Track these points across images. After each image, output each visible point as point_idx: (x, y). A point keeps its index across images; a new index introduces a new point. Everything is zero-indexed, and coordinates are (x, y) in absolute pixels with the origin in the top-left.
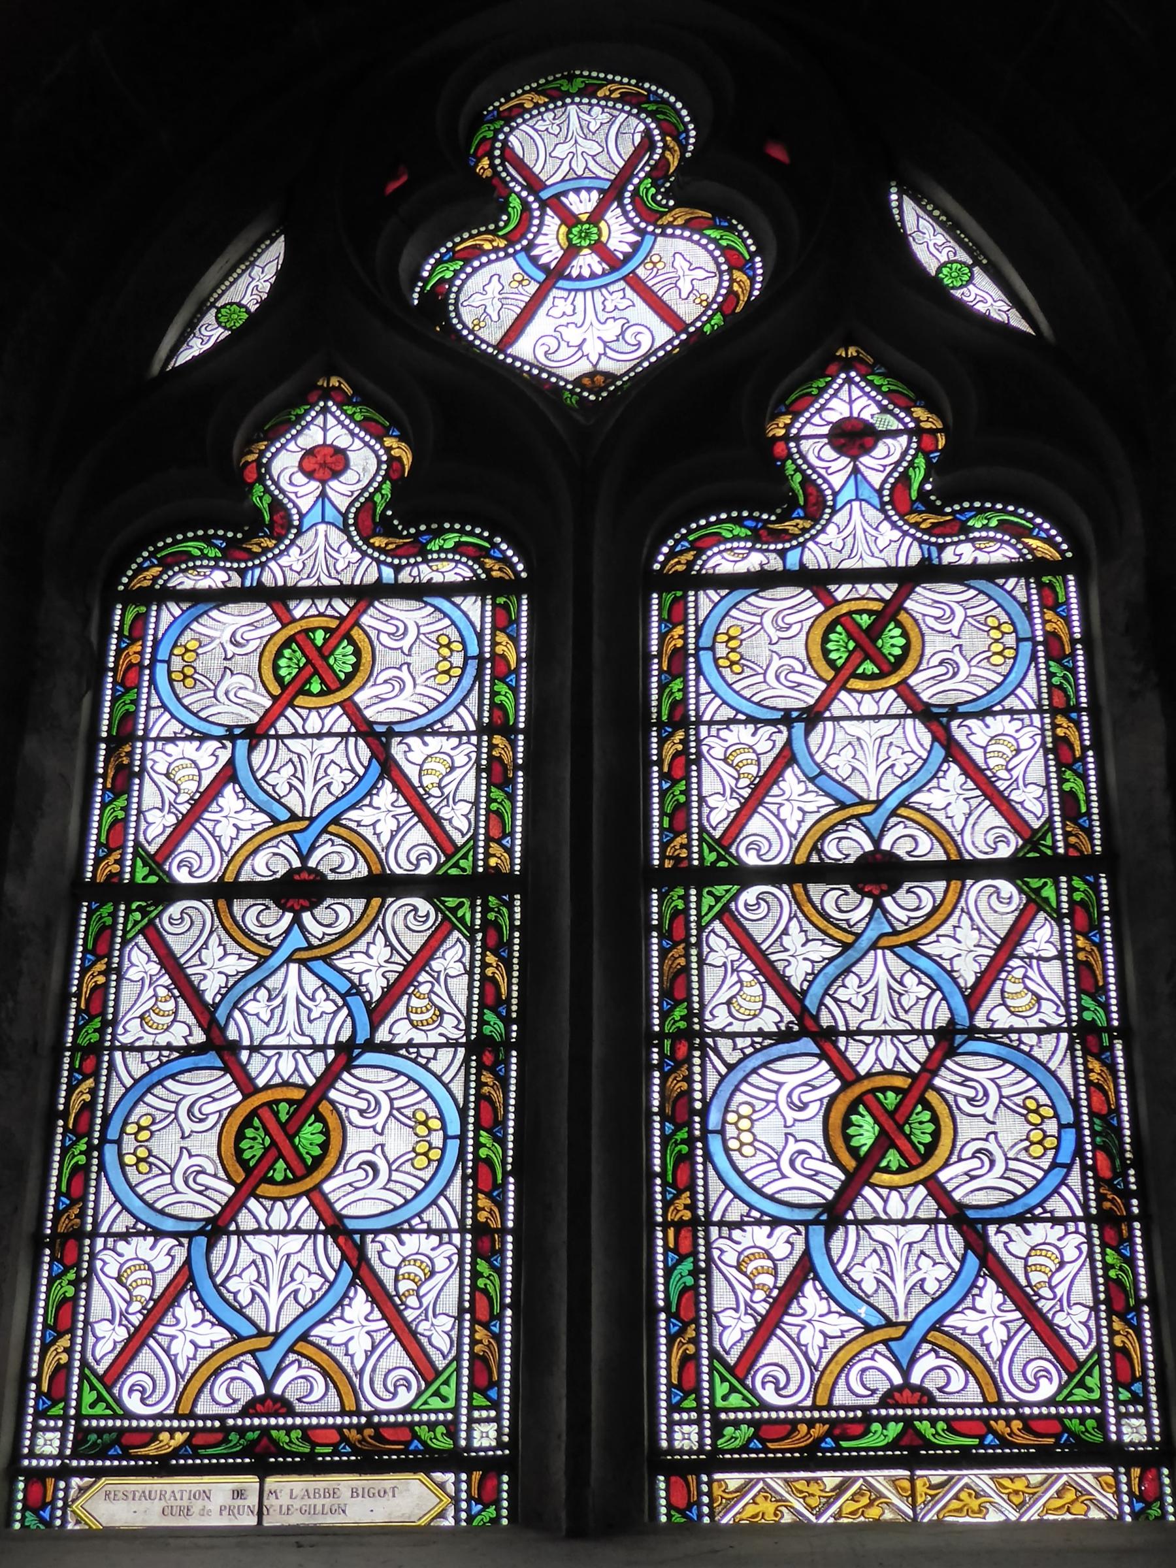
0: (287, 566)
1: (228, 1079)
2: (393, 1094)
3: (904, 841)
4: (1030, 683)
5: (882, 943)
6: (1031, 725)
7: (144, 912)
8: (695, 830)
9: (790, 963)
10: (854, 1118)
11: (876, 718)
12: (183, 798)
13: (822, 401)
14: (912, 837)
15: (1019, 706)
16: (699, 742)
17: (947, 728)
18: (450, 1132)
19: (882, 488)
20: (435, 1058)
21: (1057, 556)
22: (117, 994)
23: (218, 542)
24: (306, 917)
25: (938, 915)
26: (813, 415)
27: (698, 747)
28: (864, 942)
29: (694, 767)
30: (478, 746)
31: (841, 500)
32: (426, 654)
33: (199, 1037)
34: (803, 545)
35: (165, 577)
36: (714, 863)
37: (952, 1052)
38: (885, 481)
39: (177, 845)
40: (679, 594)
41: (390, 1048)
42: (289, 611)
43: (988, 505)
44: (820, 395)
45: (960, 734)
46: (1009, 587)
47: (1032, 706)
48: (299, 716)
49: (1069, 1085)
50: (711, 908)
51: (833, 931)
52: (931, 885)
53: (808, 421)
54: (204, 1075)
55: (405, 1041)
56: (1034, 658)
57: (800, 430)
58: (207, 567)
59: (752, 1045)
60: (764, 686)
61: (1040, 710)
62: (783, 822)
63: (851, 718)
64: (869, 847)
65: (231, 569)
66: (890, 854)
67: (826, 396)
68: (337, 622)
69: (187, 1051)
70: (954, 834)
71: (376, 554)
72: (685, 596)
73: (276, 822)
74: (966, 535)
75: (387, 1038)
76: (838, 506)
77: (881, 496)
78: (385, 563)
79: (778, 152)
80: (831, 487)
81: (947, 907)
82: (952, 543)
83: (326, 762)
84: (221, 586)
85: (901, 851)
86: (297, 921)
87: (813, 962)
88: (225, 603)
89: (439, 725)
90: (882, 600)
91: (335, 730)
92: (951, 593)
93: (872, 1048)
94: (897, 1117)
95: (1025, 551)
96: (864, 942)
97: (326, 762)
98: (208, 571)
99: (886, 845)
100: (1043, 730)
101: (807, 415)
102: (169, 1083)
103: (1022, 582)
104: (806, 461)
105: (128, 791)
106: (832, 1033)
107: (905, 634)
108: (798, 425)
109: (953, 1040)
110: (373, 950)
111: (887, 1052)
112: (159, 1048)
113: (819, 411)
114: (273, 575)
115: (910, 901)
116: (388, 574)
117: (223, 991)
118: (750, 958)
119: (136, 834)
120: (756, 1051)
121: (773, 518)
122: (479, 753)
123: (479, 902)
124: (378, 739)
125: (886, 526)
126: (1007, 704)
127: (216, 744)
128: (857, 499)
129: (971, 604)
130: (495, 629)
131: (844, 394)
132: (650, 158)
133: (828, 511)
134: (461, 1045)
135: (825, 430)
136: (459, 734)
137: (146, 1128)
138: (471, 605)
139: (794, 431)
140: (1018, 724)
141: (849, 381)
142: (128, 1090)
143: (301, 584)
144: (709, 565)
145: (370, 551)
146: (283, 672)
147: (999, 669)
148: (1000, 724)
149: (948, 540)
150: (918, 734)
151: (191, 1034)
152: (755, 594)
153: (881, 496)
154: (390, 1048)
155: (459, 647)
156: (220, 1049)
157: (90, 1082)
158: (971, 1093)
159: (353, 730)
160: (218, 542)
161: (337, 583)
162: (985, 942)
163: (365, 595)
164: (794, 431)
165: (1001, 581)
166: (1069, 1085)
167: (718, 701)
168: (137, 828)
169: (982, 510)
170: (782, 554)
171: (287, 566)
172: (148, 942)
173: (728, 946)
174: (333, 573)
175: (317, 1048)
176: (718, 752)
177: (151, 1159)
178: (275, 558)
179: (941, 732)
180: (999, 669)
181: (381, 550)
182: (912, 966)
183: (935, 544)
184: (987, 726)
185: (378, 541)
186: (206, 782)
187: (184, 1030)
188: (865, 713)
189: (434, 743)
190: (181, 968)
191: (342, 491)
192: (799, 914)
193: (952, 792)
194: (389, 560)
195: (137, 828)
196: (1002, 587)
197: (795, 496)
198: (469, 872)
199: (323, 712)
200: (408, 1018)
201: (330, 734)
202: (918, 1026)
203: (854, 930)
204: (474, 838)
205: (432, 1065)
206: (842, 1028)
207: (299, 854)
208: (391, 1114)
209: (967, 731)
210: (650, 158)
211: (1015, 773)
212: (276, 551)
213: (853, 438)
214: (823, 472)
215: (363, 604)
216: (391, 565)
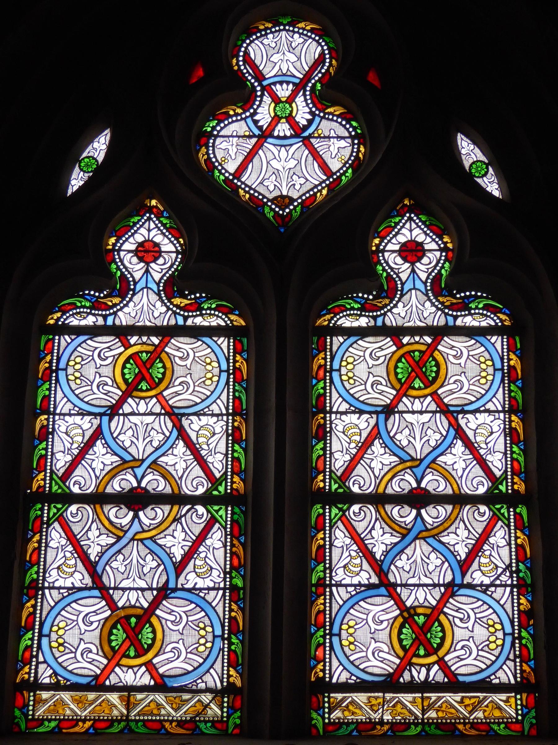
0: (399, 314)
1: (392, 602)
2: (476, 611)
3: (432, 483)
4: (500, 395)
5: (137, 537)
6: (499, 419)
7: (340, 510)
8: (48, 471)
9: (375, 545)
10: (115, 631)
11: (421, 412)
12: (75, 446)
13: (396, 230)
14: (437, 480)
15: (493, 408)
16: (54, 421)
17: (456, 419)
18: (216, 634)
19: (160, 281)
20: (495, 592)
21: (224, 324)
22: (45, 554)
23: (359, 300)
24: (141, 514)
25: (449, 522)
26: (391, 238)
27: (53, 425)
28: (130, 535)
29: (51, 436)
30: (227, 422)
31: (138, 287)
32: (201, 370)
33: (375, 580)
34: (385, 314)
35: (335, 319)
36: (336, 489)
37: (453, 595)
38: (162, 278)
39: (72, 472)
40: (51, 337)
41: (471, 586)
42: (128, 340)
43: (479, 294)
44: (395, 227)
45: (462, 422)
46: (219, 342)
47: (500, 408)
48: (136, 401)
49: (221, 615)
50: (336, 515)
51: (114, 530)
52: (446, 506)
53: (389, 241)
54: (378, 600)
55: (479, 583)
56: (502, 381)
57: (385, 247)
58: (86, 312)
59: (355, 590)
60: (91, 392)
61: (504, 411)
62: (94, 470)
63: (408, 412)
64: (414, 485)
65: (98, 315)
66: (425, 489)
67: (399, 227)
68: (426, 347)
69: (370, 586)
70: (457, 479)
71: (175, 309)
72: (53, 339)
73: (402, 461)
74: (201, 311)
75: (470, 581)
76: (137, 290)
77: (426, 286)
78: (179, 314)
79: (372, 78)
80: (400, 279)
81: (453, 517)
82: (193, 316)
83: (149, 428)
84: (366, 325)
85: (430, 488)
86: (136, 516)
87: (102, 546)
88: (367, 336)
89: (207, 409)
90: (153, 345)
91: (429, 409)
92: (461, 343)
93: (414, 592)
94: (424, 629)
95: (498, 321)
96: (130, 535)
97: (149, 428)
98: (85, 315)
99: (423, 485)
100: (504, 421)
101: (388, 238)
102: (74, 605)
103: (500, 338)
104: (123, 264)
105: (47, 440)
106: (395, 585)
107: (164, 367)
108: (383, 244)
109: (453, 589)
110: (176, 534)
111: (421, 594)
112: (355, 586)
113: (395, 236)
114: (391, 320)
115: (434, 513)
116: (181, 321)
117: (100, 555)
118: (355, 543)
119: (51, 466)
120: (357, 593)
121: (371, 297)
122: (227, 426)
123: (230, 508)
124: (175, 415)
125: (428, 304)
126: (487, 406)
127: (369, 416)
128: (414, 288)
129: (198, 349)
130: (235, 353)
131: (407, 226)
132: (250, 74)
133: (131, 293)
134: (508, 586)
135: (397, 247)
136: (217, 415)
137: (352, 627)
138: (223, 342)
139: (381, 247)
140: (492, 418)
141: (410, 219)
142: (341, 607)
143: (406, 325)
144: (339, 323)
145: (171, 307)
146: (127, 376)
147: (209, 388)
148: (482, 418)
149: (190, 314)
150: (442, 423)
151: (83, 579)
152: (91, 339)
153: (426, 286)
154: (471, 586)
155: (217, 365)
156: (385, 585)
157: (33, 602)
158: (461, 616)
159: (163, 411)
160: (359, 300)
161: (425, 325)
162: (471, 536)
163: (438, 333)
164: (381, 247)
165: (489, 337)
166: (221, 615)
167: (65, 399)
168: (51, 462)
169: (476, 297)
170: (105, 317)
171: (399, 314)
172: (61, 525)
173: (345, 536)
174: (423, 319)
175: (434, 585)
176: (63, 429)
177: (356, 643)
178: (121, 309)
179: (453, 422)
180: (209, 388)
181: (177, 306)
182: (434, 549)
183: (451, 315)
184: (477, 419)
185: (177, 301)
186: (87, 437)
187: (366, 576)
188: (415, 409)
189: (204, 419)
190: (78, 541)
191: (159, 270)
192: (97, 520)
193: (457, 456)
194: (182, 313)
195: (51, 462)
196: (489, 340)
197: (382, 285)
198: (223, 492)
199: (147, 400)
200: (480, 570)
201: (426, 412)
202: (437, 582)
203: (124, 529)
204: (226, 473)
205: (494, 595)
206: (399, 582)
207: (416, 480)
208: (475, 621)
209: (190, 422)
210: (250, 74)
211: (489, 445)
212: (122, 305)
213: (412, 252)
214: (130, 270)
215: (166, 340)
216: (451, 315)
